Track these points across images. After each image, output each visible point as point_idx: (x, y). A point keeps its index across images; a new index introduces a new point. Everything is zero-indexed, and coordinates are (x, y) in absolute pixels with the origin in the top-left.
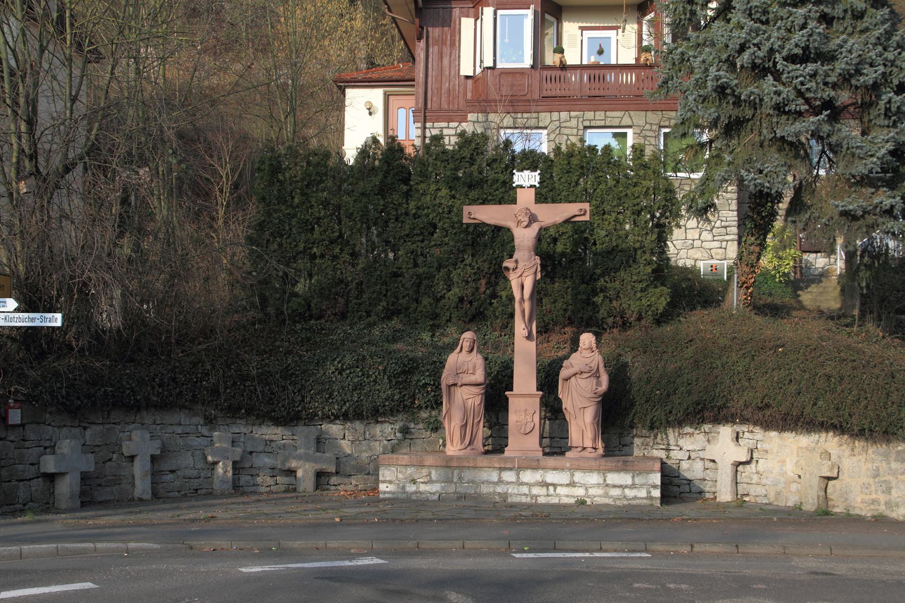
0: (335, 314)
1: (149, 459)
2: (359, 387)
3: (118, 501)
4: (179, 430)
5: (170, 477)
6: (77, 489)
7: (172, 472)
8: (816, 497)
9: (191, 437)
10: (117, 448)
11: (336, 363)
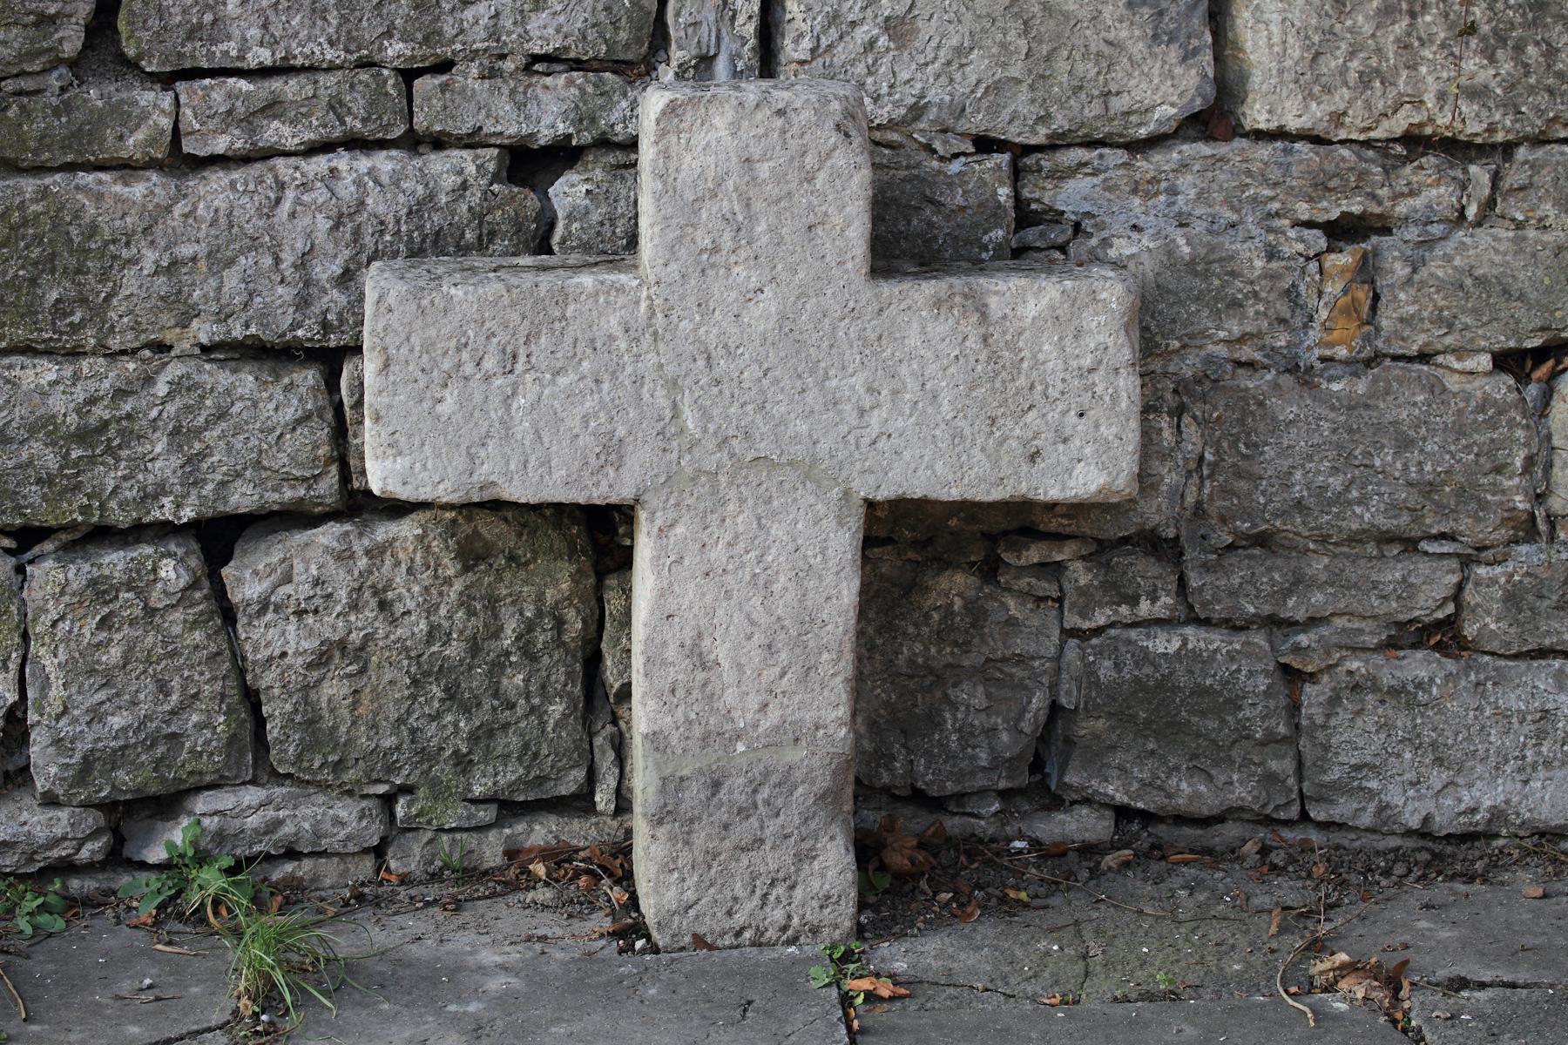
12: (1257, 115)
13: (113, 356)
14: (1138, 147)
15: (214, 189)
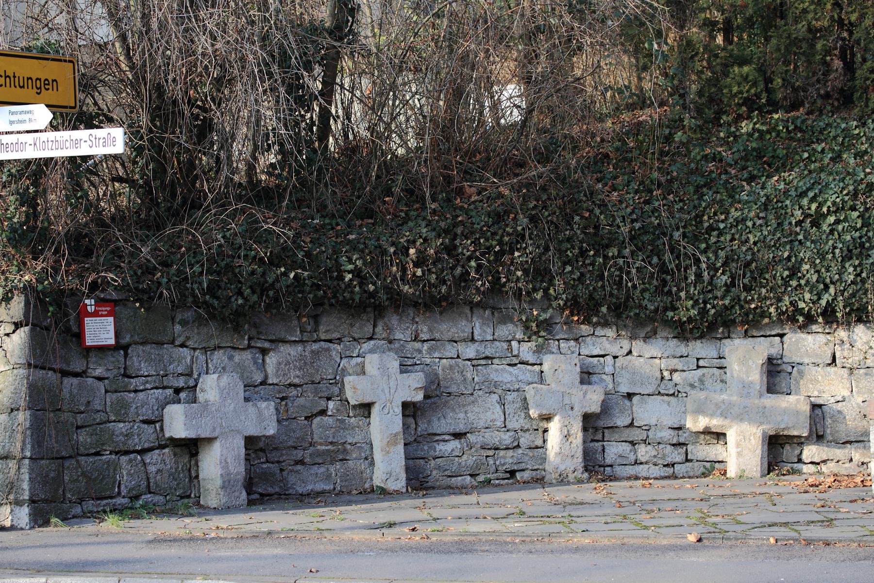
0: (827, 96)
1: (399, 410)
2: (855, 252)
3: (341, 492)
4: (470, 351)
5: (454, 445)
6: (239, 469)
7: (458, 436)
8: (822, 402)
9: (497, 364)
10: (336, 390)
11: (805, 202)
12: (270, 381)
13: (130, 422)
14: (255, 386)
15: (141, 395)
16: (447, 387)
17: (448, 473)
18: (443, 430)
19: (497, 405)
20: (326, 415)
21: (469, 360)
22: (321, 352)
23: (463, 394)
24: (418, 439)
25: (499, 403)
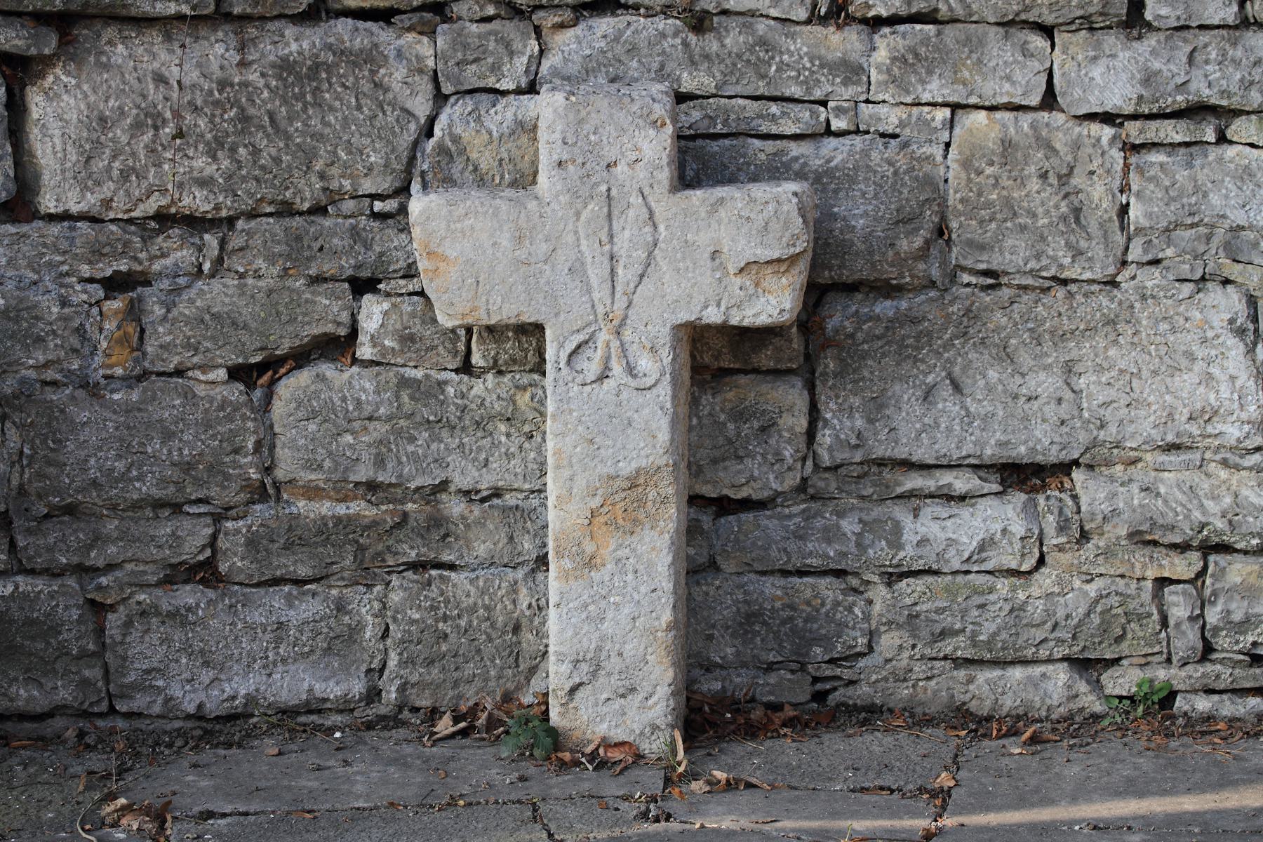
12: (48, 203)
16: (982, 247)
17: (958, 646)
18: (947, 447)
19: (1232, 341)
20: (355, 361)
21: (1107, 118)
22: (329, 68)
23: (1065, 282)
24: (819, 483)
25: (1241, 332)
